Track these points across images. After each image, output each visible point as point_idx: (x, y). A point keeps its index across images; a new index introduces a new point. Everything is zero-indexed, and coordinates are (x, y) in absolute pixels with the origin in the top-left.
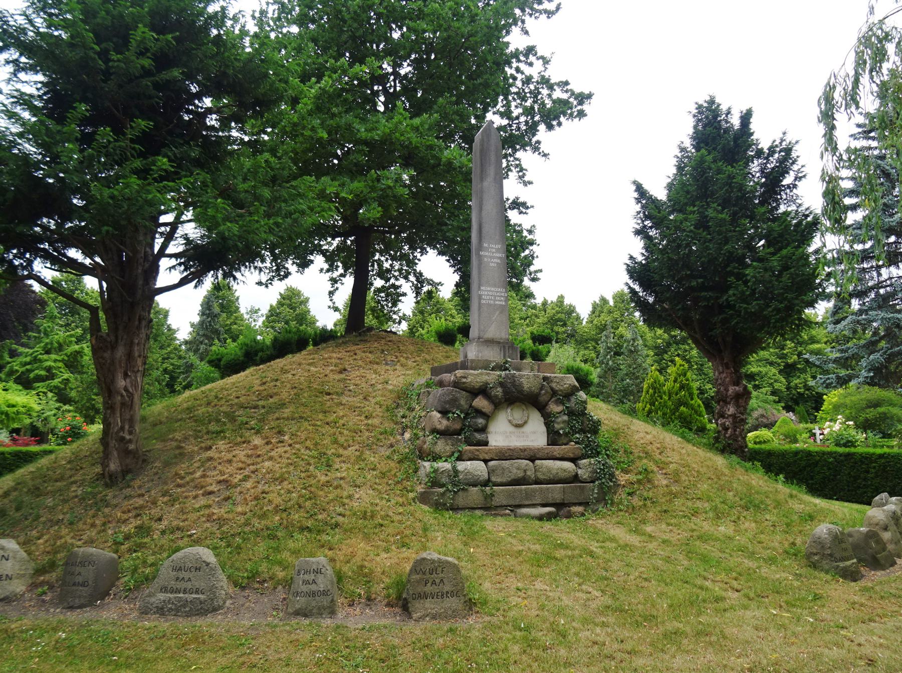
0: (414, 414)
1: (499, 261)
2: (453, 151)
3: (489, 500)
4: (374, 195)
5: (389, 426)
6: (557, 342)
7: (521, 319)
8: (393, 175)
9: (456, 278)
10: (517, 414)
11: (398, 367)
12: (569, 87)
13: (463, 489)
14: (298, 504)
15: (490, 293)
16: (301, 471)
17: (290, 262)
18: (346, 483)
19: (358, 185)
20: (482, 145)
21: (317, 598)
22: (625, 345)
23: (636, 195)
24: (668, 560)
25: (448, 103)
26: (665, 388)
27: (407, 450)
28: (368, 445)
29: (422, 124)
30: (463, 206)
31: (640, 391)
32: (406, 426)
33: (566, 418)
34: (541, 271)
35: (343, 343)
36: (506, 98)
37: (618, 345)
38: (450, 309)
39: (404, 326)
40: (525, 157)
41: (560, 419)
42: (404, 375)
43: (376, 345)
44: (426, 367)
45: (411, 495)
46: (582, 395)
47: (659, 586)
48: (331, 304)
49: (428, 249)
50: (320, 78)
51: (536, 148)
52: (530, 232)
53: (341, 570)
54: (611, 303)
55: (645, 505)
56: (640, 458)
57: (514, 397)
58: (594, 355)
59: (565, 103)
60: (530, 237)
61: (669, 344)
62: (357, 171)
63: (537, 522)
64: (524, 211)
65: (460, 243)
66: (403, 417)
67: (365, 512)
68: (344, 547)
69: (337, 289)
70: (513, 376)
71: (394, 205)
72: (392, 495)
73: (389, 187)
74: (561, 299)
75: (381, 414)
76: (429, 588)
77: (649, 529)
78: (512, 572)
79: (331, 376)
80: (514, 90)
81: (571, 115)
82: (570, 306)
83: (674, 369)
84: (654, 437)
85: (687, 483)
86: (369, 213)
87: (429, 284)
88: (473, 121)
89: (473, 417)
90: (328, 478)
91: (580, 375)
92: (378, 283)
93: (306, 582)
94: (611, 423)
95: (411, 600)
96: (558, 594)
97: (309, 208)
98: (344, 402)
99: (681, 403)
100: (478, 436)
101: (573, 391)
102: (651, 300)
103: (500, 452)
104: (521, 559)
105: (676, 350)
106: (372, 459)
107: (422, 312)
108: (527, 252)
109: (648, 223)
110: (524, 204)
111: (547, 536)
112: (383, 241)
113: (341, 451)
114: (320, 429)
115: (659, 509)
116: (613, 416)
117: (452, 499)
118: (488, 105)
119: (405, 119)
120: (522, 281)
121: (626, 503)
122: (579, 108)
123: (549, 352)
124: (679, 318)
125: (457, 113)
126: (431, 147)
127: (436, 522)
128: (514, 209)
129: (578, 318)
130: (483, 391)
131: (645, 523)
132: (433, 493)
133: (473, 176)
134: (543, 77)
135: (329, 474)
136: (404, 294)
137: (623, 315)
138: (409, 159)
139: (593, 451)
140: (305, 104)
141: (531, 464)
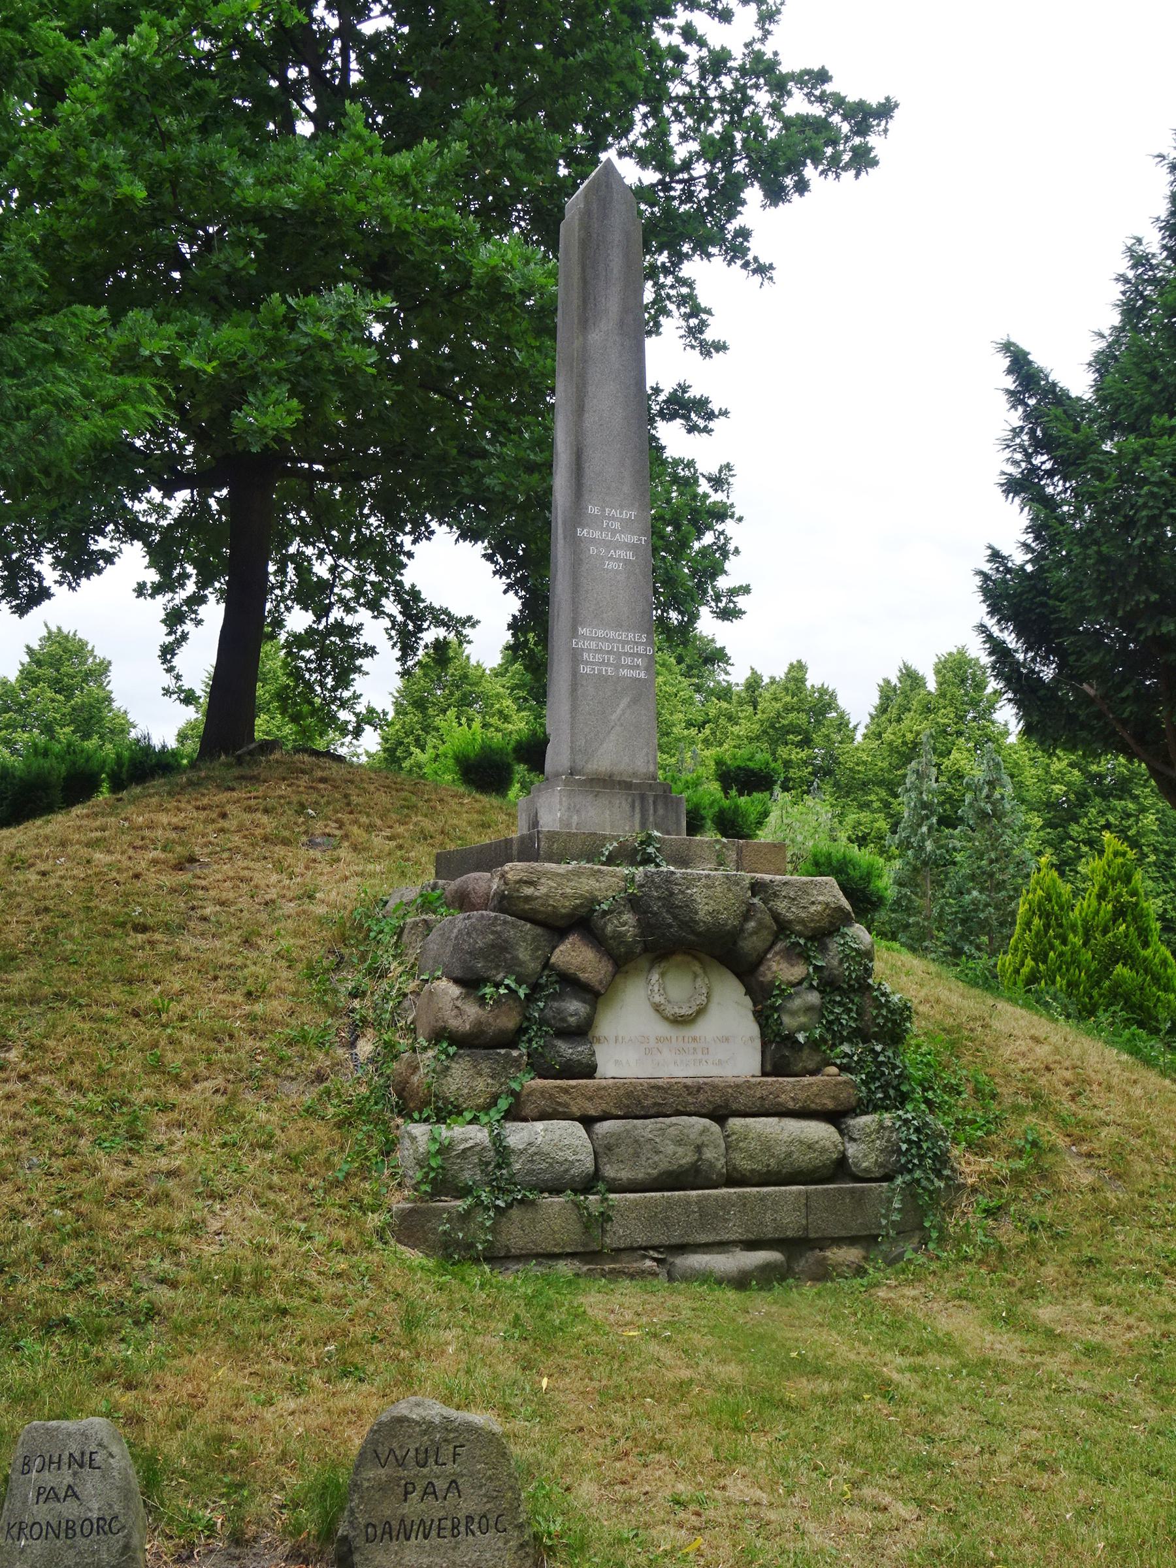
0: (384, 985)
1: (630, 555)
2: (505, 249)
3: (597, 1232)
4: (278, 364)
5: (311, 1019)
6: (785, 789)
7: (690, 724)
8: (331, 309)
9: (513, 604)
10: (678, 986)
11: (344, 853)
12: (829, 88)
13: (521, 1202)
14: (39, 1251)
15: (605, 646)
16: (53, 1154)
17: (48, 559)
18: (184, 1187)
19: (233, 335)
20: (586, 227)
21: (80, 1541)
22: (968, 797)
23: (1010, 382)
24: (1102, 1405)
25: (492, 113)
26: (1075, 915)
27: (364, 1090)
28: (250, 1077)
29: (418, 169)
30: (534, 393)
31: (1007, 920)
32: (364, 1020)
33: (814, 998)
34: (746, 590)
35: (190, 783)
36: (655, 112)
37: (950, 798)
38: (498, 696)
39: (371, 741)
40: (707, 274)
41: (797, 1003)
42: (361, 874)
43: (283, 789)
44: (424, 854)
45: (374, 1220)
46: (859, 933)
47: (1081, 1484)
48: (168, 681)
49: (434, 525)
50: (124, 32)
51: (737, 250)
52: (718, 482)
53: (156, 1448)
54: (932, 685)
55: (1033, 1244)
56: (1018, 1110)
57: (670, 939)
58: (883, 824)
59: (820, 126)
60: (716, 497)
61: (1083, 799)
62: (232, 297)
63: (731, 1294)
64: (701, 423)
65: (523, 508)
66: (355, 994)
67: (237, 1275)
68: (170, 1380)
69: (184, 637)
70: (668, 878)
71: (336, 396)
72: (317, 1222)
73: (325, 345)
74: (797, 671)
75: (291, 987)
76: (414, 1507)
77: (1046, 1313)
78: (659, 1448)
79: (153, 878)
80: (677, 89)
81: (835, 161)
82: (823, 691)
83: (1098, 864)
84: (1057, 1050)
85: (1148, 1180)
86: (270, 415)
87: (439, 623)
88: (563, 172)
89: (554, 997)
90: (130, 1174)
91: (850, 879)
92: (298, 620)
93: (48, 1494)
94: (936, 1013)
95: (359, 1542)
96: (794, 1513)
97: (87, 394)
98: (186, 950)
99: (1116, 955)
100: (567, 1050)
101: (836, 922)
102: (1048, 673)
103: (629, 1095)
104: (684, 1408)
105: (1102, 813)
106: (262, 1116)
107: (420, 704)
108: (708, 538)
109: (1042, 461)
110: (701, 406)
111: (762, 1337)
112: (309, 500)
113: (172, 1094)
114: (112, 1029)
115: (1072, 1255)
116: (944, 994)
117: (493, 1230)
118: (607, 128)
119: (370, 151)
120: (694, 617)
121: (980, 1238)
122: (857, 141)
123: (766, 814)
124: (1124, 723)
125: (515, 142)
126: (444, 236)
127: (442, 1299)
128: (672, 417)
129: (842, 724)
130: (581, 922)
131: (1033, 1297)
132: (437, 1213)
133: (559, 319)
134: (758, 57)
135: (135, 1160)
136: (370, 651)
137: (961, 718)
138: (383, 266)
139: (889, 1092)
140: (84, 101)
141: (715, 1127)
